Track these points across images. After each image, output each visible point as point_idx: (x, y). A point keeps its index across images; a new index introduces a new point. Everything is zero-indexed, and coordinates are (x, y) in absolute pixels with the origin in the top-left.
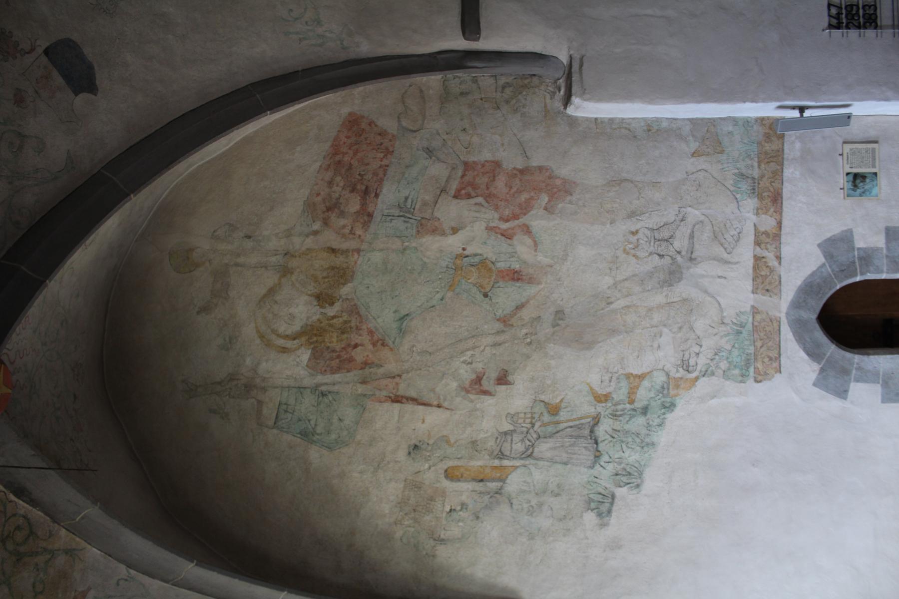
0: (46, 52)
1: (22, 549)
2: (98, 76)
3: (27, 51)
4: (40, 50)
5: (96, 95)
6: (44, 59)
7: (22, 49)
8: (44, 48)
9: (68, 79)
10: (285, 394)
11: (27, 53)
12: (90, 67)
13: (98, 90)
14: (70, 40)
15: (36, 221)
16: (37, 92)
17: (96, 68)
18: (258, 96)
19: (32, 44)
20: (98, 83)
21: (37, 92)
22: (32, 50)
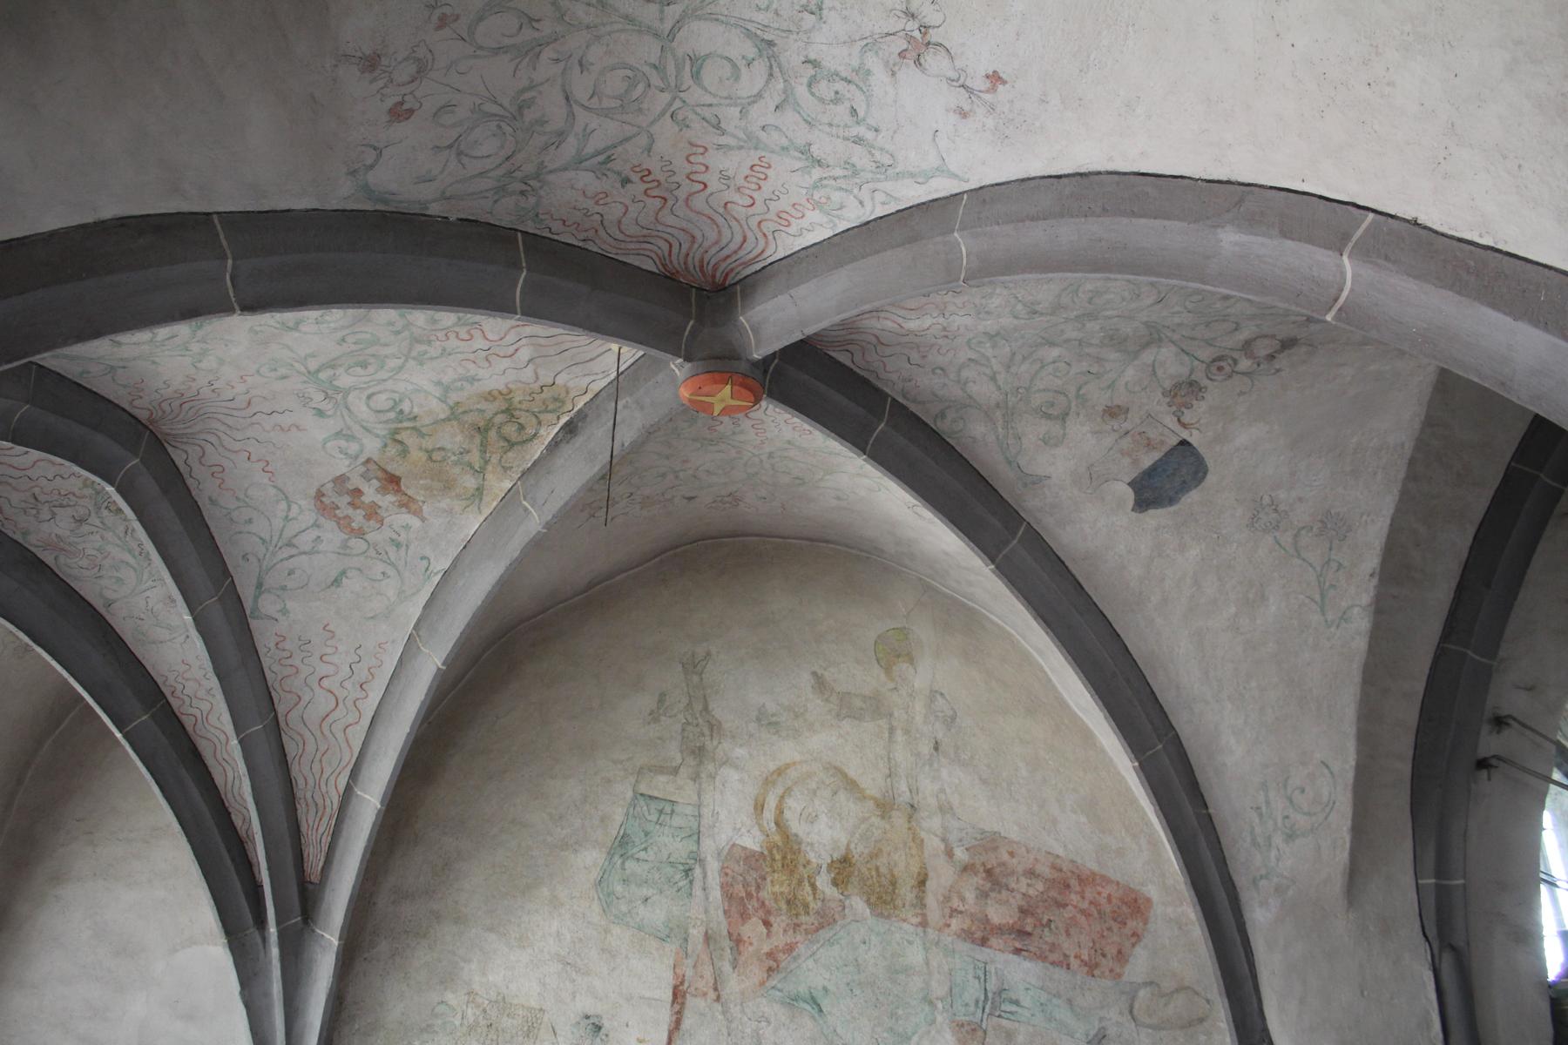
0: (1184, 443)
1: (493, 434)
2: (1160, 511)
3: (1182, 419)
4: (1185, 435)
5: (1133, 510)
6: (1174, 441)
7: (1183, 413)
8: (1189, 439)
9: (1151, 472)
10: (689, 810)
11: (1179, 420)
12: (1172, 501)
13: (1140, 512)
14: (1205, 473)
15: (948, 440)
16: (1127, 433)
17: (1172, 509)
18: (1160, 746)
19: (1192, 424)
20: (1151, 512)
21: (1127, 433)
22: (1184, 426)
